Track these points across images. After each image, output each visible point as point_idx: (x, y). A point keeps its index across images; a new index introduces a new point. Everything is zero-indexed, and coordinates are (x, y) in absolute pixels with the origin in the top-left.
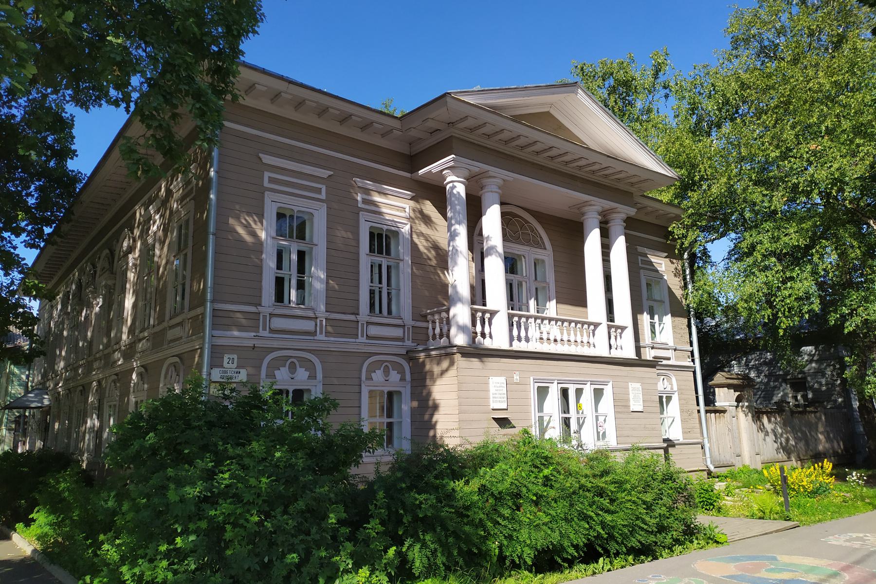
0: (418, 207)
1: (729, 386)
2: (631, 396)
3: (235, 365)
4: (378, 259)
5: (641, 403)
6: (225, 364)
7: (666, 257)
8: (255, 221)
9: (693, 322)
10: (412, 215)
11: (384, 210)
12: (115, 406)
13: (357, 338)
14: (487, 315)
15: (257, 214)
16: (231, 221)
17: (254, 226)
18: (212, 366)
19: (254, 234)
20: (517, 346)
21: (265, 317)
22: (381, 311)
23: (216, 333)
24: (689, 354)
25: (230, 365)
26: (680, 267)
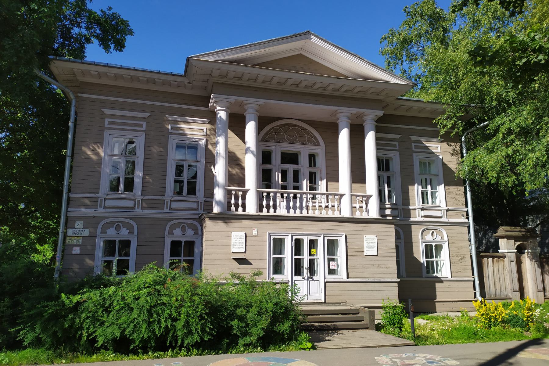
0: (213, 127)
1: (508, 238)
2: (365, 244)
3: (82, 227)
6: (76, 227)
7: (442, 142)
8: (98, 147)
9: (468, 189)
10: (208, 133)
11: (188, 132)
15: (100, 143)
16: (84, 148)
17: (98, 150)
19: (97, 154)
20: (358, 215)
21: (167, 202)
24: (465, 214)
25: (79, 227)
26: (458, 148)
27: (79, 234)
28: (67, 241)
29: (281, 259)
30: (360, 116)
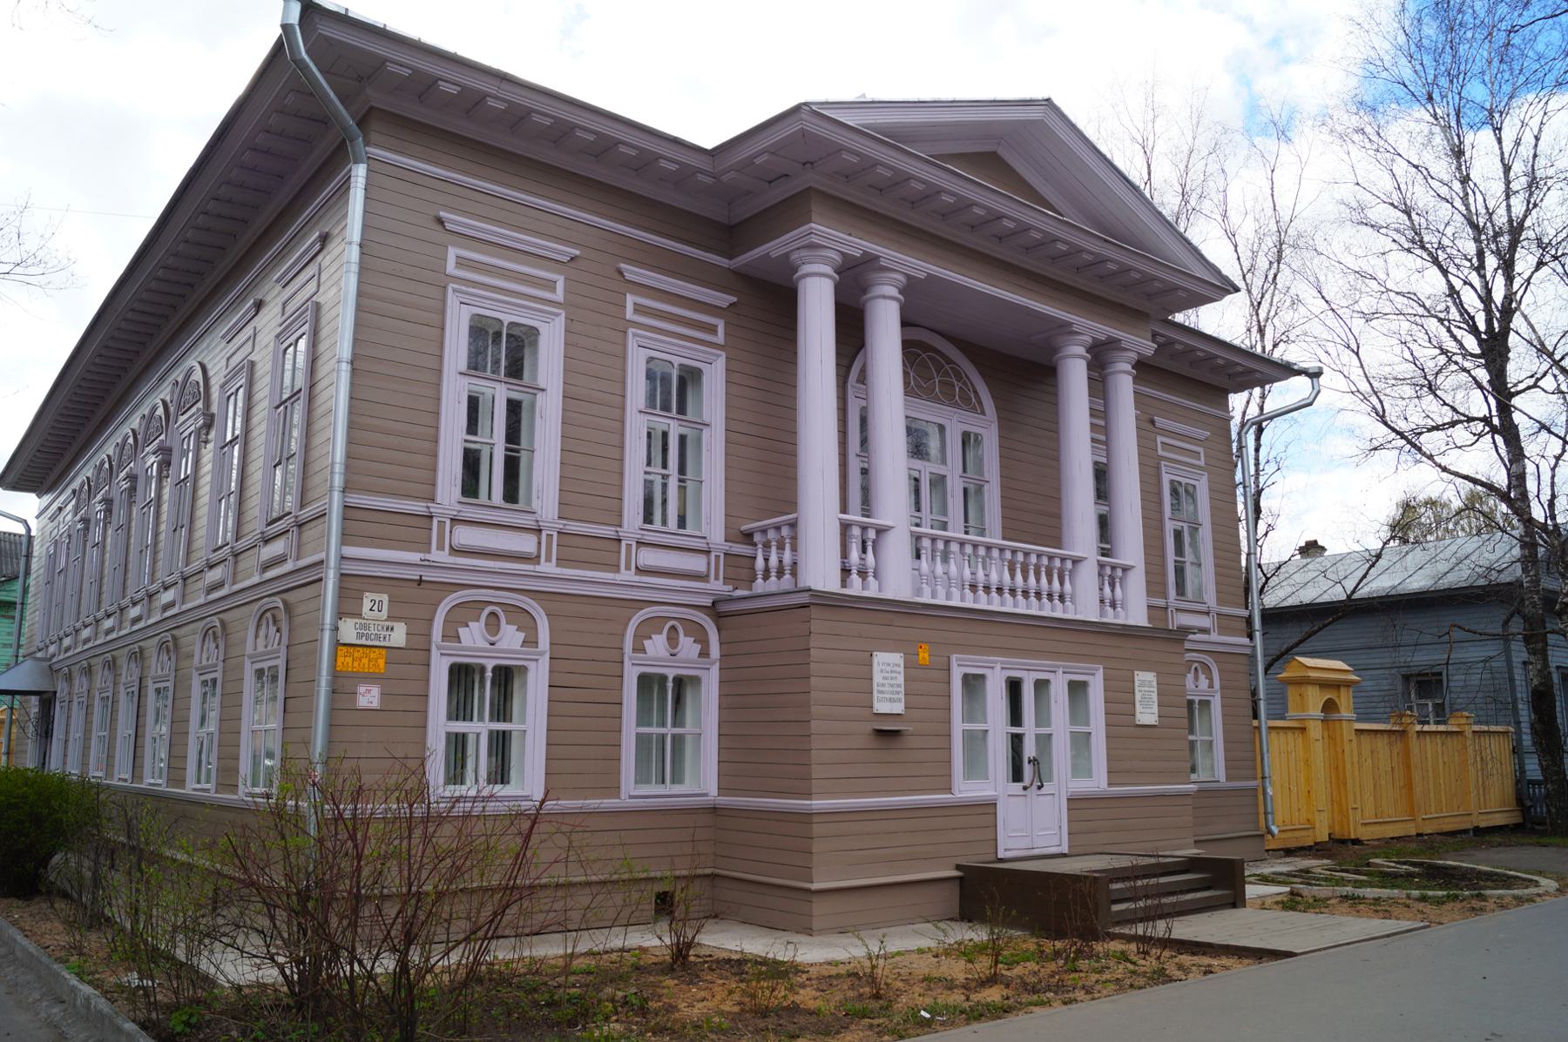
4: (661, 422)
5: (1155, 709)
12: (214, 681)
13: (618, 571)
14: (1119, 573)
18: (340, 614)
21: (629, 546)
22: (664, 522)
23: (350, 551)
24: (1243, 625)
27: (378, 637)
28: (340, 660)
29: (1013, 724)
30: (869, 261)
